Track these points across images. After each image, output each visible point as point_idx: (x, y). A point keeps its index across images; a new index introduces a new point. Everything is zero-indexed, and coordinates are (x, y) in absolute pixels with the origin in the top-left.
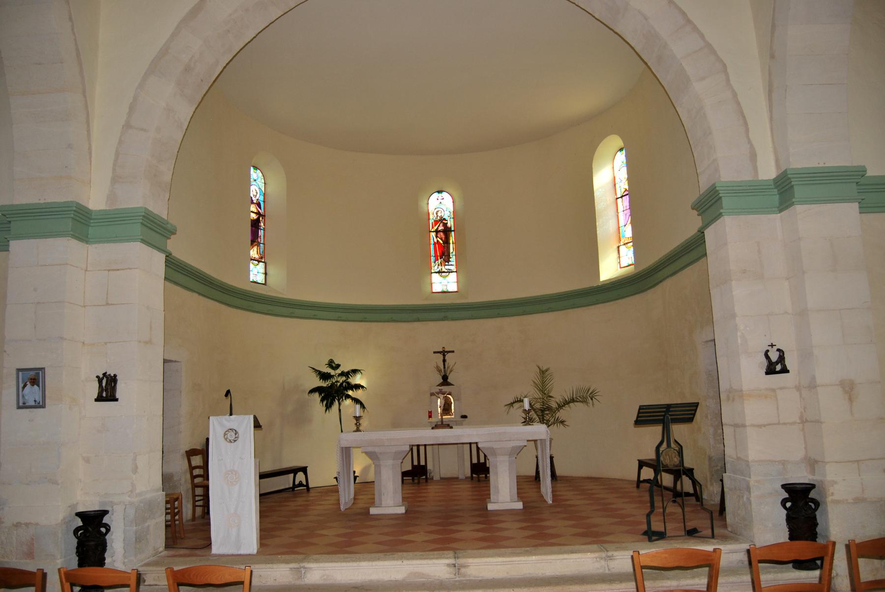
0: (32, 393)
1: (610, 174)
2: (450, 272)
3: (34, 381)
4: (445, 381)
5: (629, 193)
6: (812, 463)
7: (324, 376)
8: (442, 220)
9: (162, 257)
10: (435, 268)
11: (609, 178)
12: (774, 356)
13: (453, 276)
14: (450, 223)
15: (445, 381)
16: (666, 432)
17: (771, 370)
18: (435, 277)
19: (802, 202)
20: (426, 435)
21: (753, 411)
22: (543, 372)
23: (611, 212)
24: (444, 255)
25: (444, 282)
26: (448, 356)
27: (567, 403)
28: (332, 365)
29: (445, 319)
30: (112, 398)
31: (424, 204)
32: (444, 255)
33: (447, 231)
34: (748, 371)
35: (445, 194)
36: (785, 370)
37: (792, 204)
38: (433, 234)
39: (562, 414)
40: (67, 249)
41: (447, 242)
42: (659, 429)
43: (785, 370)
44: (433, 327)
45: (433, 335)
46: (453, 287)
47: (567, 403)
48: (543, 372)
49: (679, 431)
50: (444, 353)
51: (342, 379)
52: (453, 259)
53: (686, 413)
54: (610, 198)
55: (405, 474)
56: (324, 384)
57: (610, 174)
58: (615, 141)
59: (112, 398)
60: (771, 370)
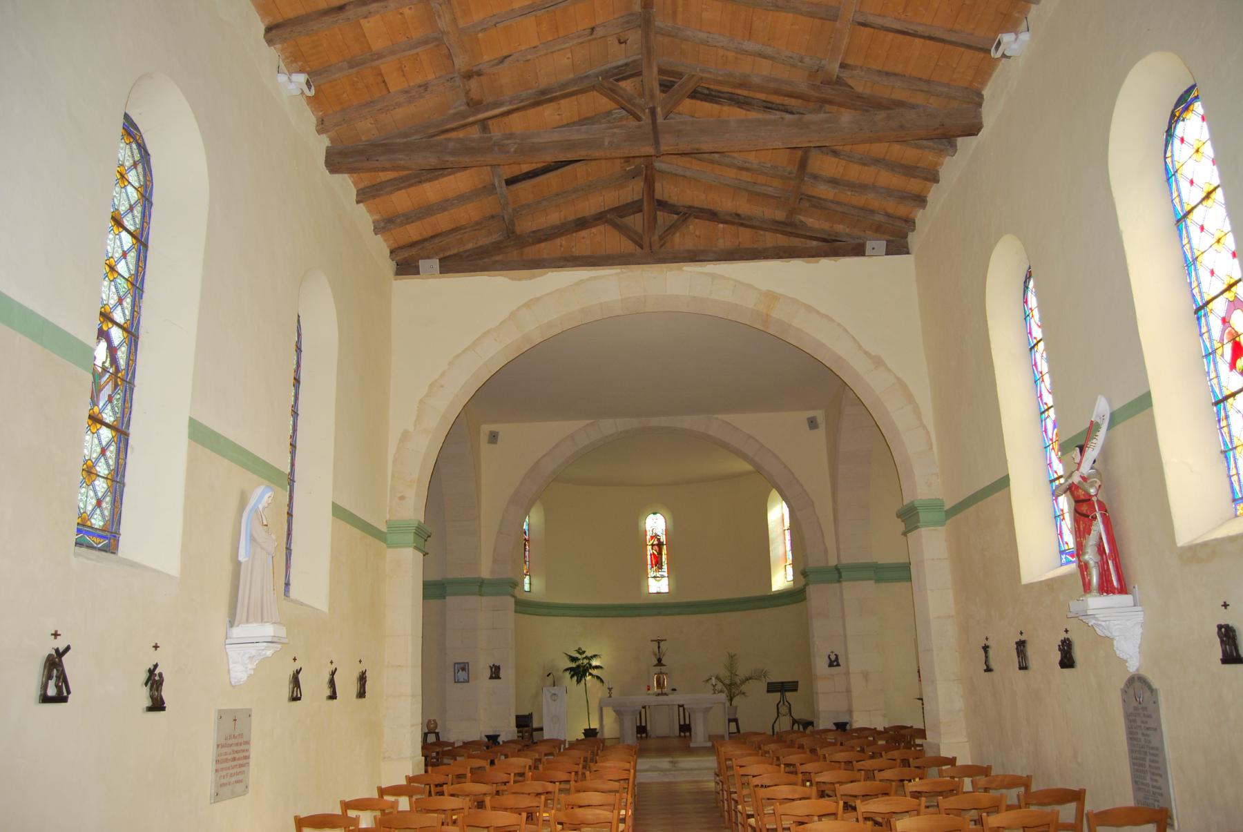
0: (462, 675)
1: (778, 514)
2: (663, 577)
3: (463, 669)
4: (660, 662)
5: (791, 529)
6: (850, 712)
7: (573, 659)
8: (655, 536)
9: (513, 600)
10: (651, 574)
11: (779, 515)
12: (833, 658)
13: (665, 581)
14: (663, 539)
15: (660, 662)
16: (783, 695)
17: (831, 665)
18: (651, 581)
19: (928, 524)
20: (651, 700)
21: (821, 686)
22: (732, 657)
23: (781, 538)
24: (658, 563)
25: (658, 584)
26: (662, 644)
27: (747, 679)
28: (580, 652)
29: (659, 614)
30: (499, 678)
31: (641, 524)
32: (658, 563)
33: (660, 545)
34: (821, 664)
35: (658, 515)
36: (838, 665)
37: (917, 527)
38: (649, 548)
39: (744, 688)
40: (472, 601)
41: (660, 553)
42: (779, 694)
43: (838, 665)
44: (650, 621)
45: (651, 626)
46: (665, 589)
47: (747, 679)
48: (732, 657)
49: (789, 695)
50: (659, 641)
51: (586, 662)
52: (665, 567)
53: (792, 686)
54: (780, 530)
55: (973, 130)
56: (573, 665)
57: (778, 514)
58: (774, 494)
59: (499, 678)
60: (831, 665)
